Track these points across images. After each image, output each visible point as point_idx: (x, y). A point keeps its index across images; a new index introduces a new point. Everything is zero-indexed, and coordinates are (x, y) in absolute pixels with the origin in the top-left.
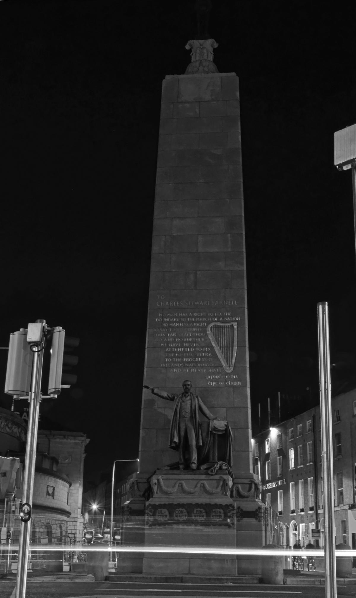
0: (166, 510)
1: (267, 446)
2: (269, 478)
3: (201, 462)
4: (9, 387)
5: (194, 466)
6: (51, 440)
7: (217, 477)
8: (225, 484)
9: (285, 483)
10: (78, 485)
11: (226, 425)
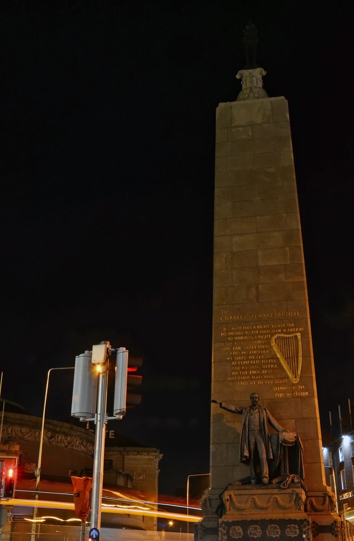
0: (239, 527)
1: (340, 455)
2: (344, 488)
3: (272, 476)
4: (76, 409)
6: (125, 456)
7: (290, 491)
8: (298, 498)
11: (296, 437)
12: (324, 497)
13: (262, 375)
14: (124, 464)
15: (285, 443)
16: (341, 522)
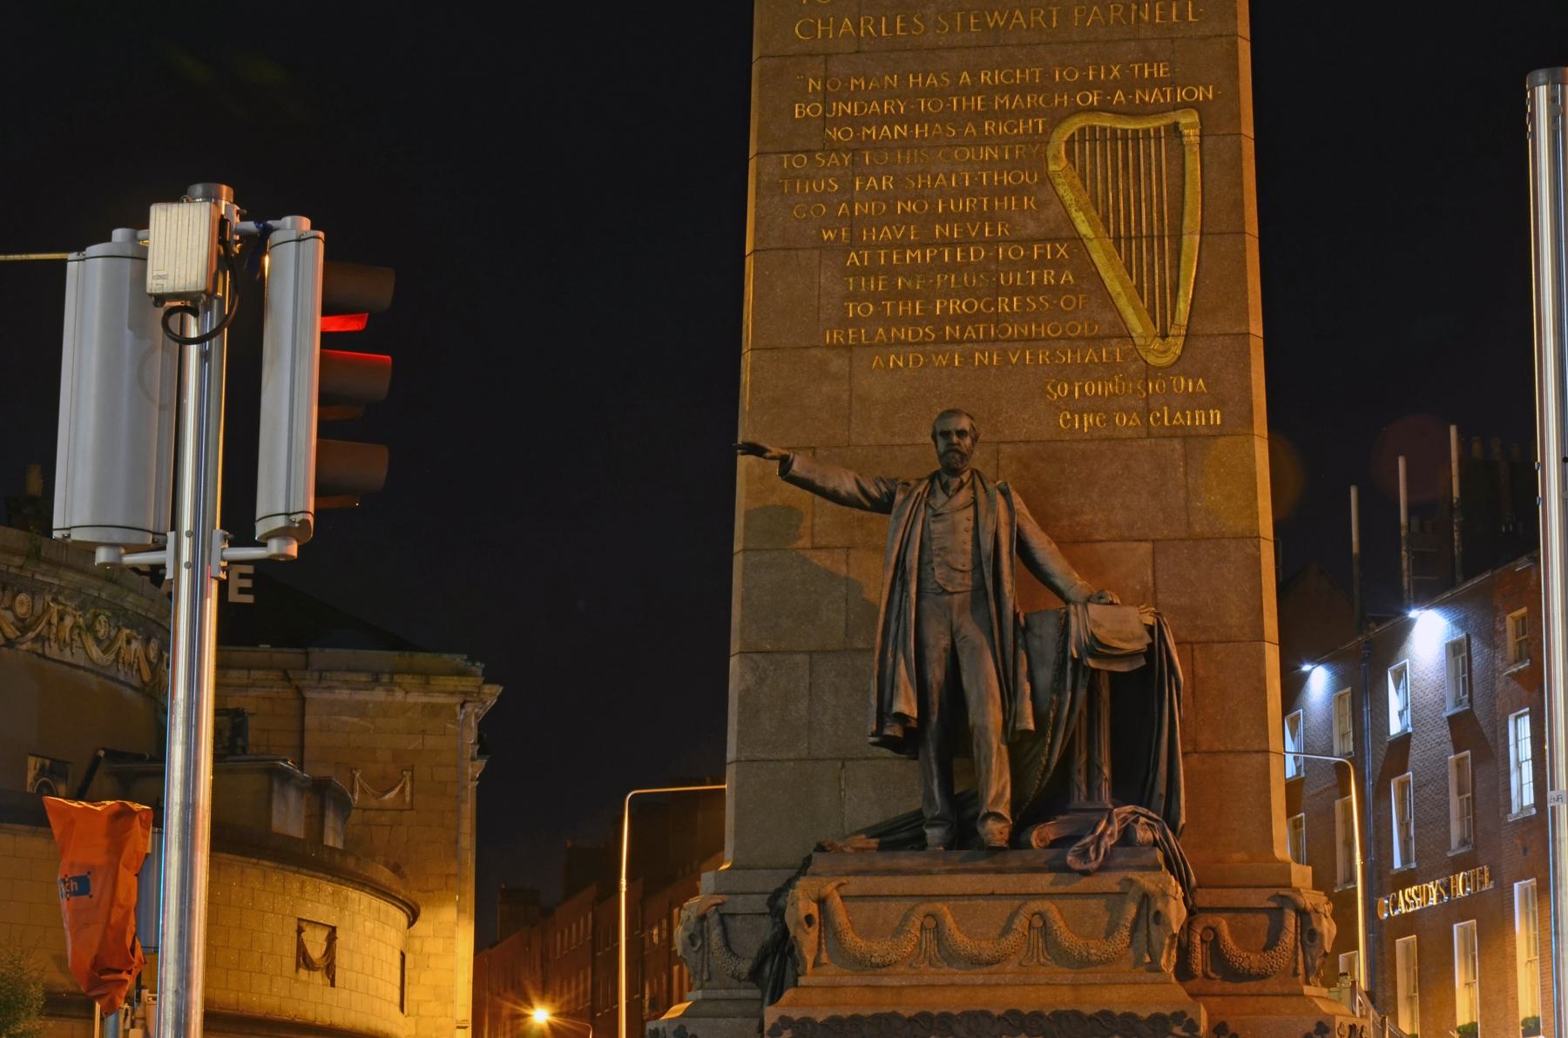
1: (1395, 702)
2: (1406, 859)
3: (1026, 814)
4: (78, 501)
5: (995, 832)
6: (309, 694)
7: (1110, 881)
8: (1148, 910)
9: (1488, 886)
10: (449, 914)
11: (1150, 629)
12: (1276, 915)
13: (998, 319)
14: (302, 731)
15: (1095, 655)
16: (1352, 1027)
